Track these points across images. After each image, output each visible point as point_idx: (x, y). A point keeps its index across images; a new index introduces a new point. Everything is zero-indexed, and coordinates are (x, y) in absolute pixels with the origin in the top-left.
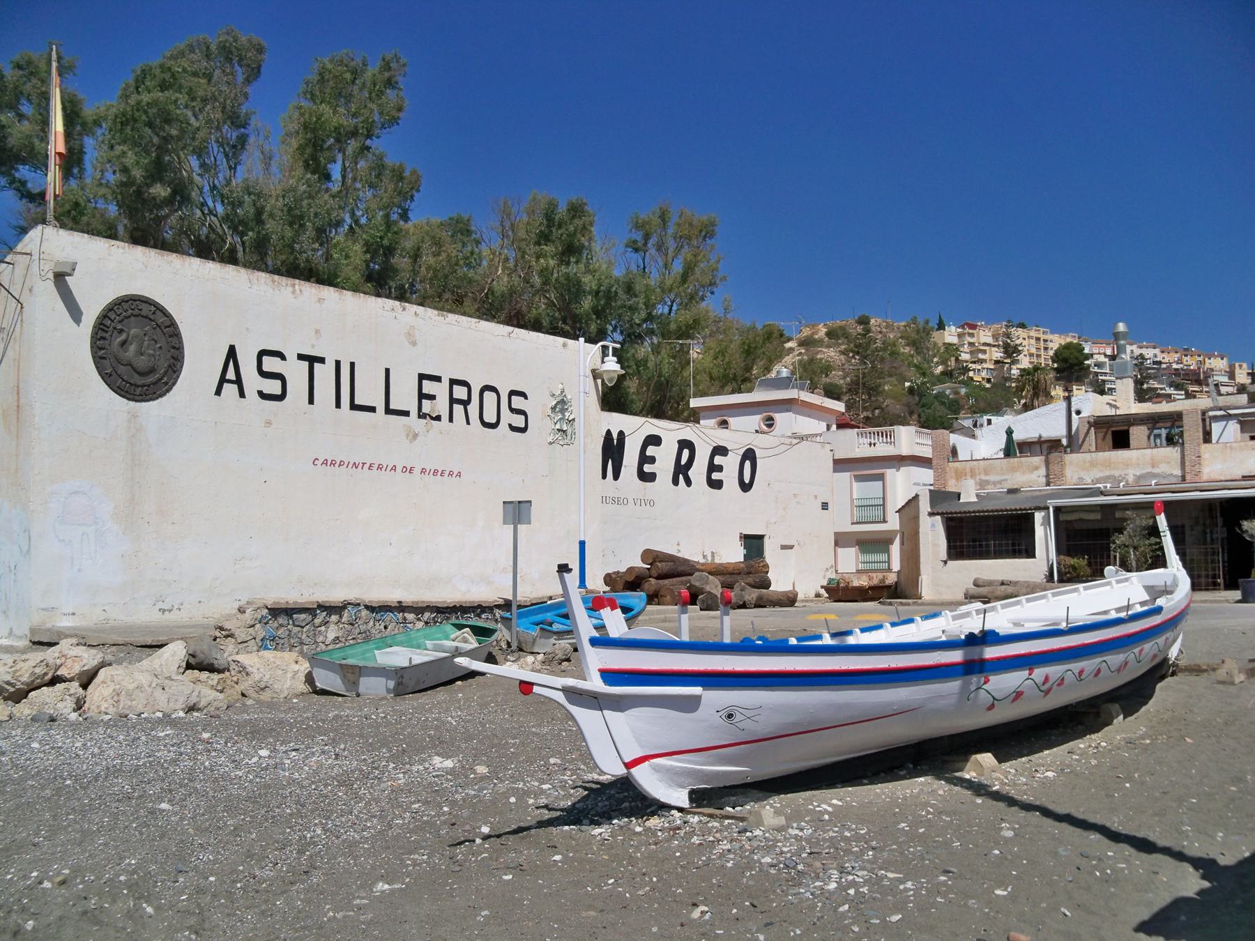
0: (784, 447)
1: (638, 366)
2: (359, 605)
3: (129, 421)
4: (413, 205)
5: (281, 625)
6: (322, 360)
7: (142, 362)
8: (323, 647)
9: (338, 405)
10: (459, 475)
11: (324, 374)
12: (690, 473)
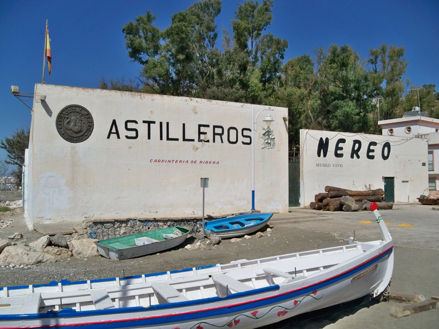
0: (403, 141)
1: (372, 108)
2: (136, 220)
3: (72, 150)
4: (285, 53)
5: (99, 228)
6: (154, 122)
7: (76, 129)
8: (119, 236)
9: (161, 139)
10: (218, 163)
11: (155, 128)
12: (359, 153)
